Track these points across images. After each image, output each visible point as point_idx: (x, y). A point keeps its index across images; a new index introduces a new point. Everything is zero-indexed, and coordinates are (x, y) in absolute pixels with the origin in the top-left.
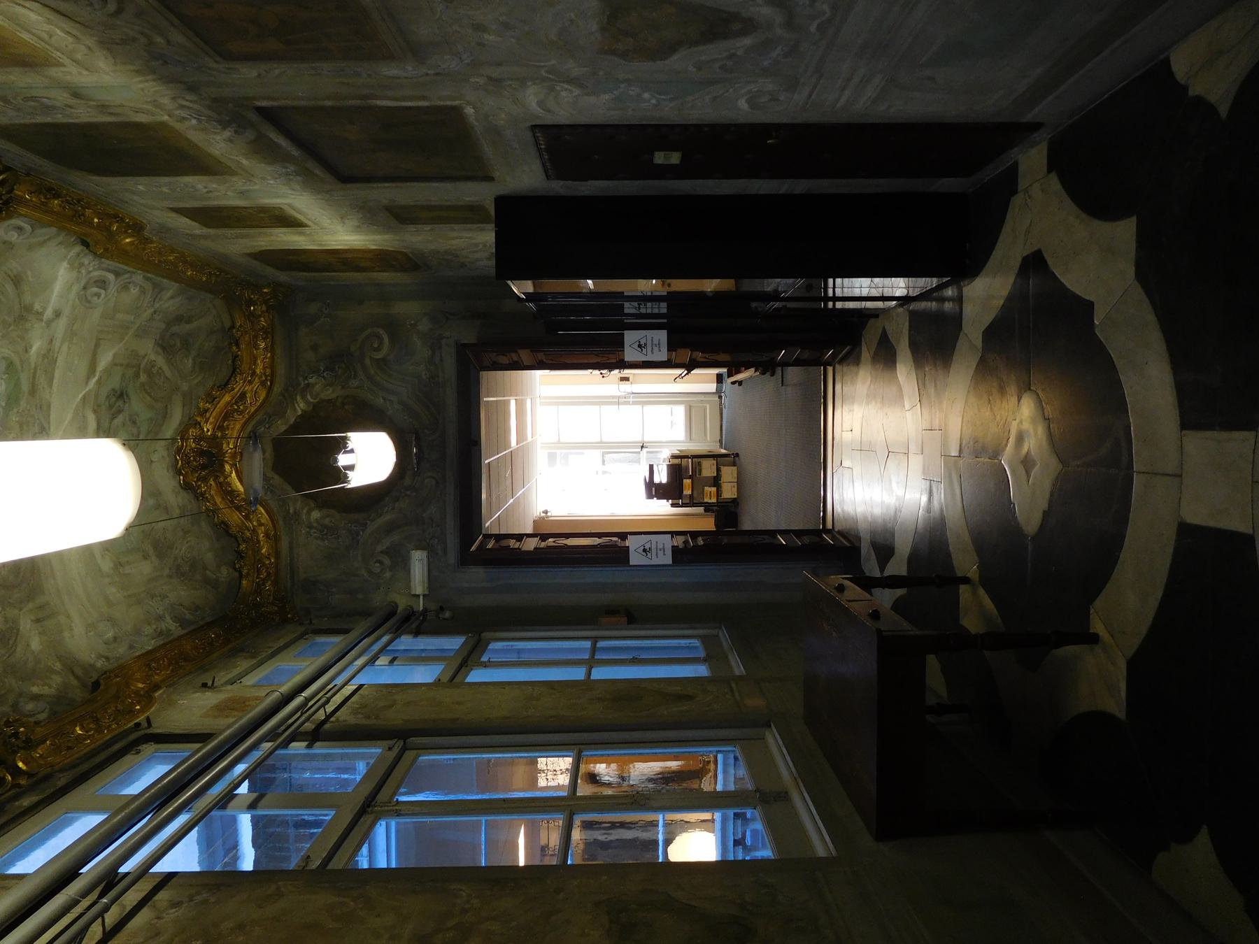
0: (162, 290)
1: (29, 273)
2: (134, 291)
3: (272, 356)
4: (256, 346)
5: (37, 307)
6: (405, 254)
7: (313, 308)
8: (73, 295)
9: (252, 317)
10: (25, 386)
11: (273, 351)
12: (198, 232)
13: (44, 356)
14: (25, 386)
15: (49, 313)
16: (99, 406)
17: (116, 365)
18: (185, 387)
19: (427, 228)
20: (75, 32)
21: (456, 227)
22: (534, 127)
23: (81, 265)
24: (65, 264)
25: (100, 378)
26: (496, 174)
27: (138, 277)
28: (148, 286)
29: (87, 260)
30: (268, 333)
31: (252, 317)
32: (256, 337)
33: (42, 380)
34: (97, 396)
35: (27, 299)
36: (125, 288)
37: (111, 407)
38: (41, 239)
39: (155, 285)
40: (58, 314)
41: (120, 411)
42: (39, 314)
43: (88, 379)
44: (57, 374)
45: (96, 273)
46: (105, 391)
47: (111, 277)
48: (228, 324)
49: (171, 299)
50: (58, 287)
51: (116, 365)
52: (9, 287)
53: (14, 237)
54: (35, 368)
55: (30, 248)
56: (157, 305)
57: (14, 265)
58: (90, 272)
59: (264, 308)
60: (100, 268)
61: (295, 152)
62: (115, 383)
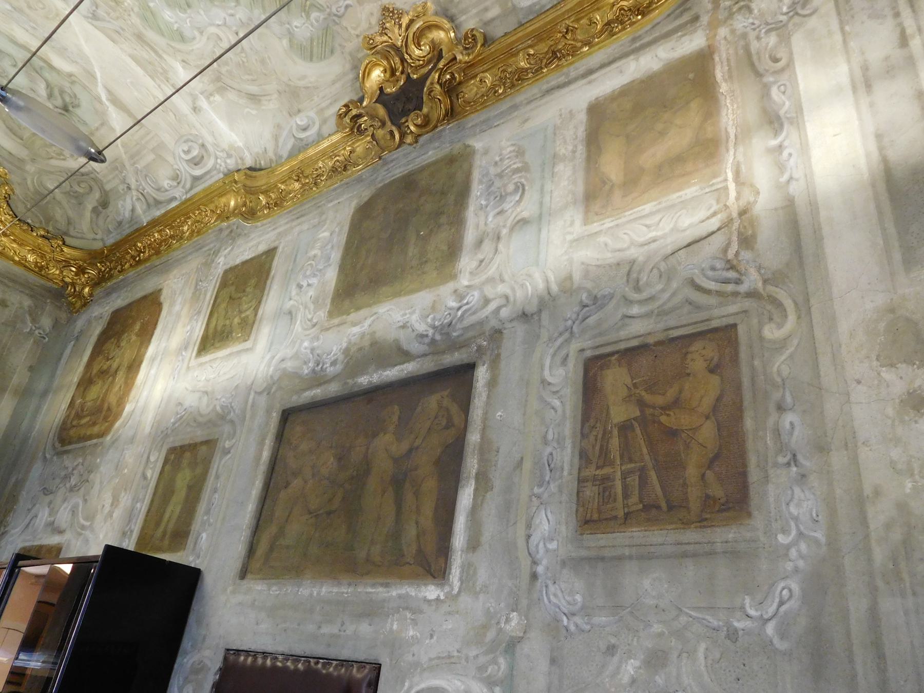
0: (148, 205)
1: (254, 112)
2: (166, 183)
3: (13, 260)
4: (33, 251)
5: (217, 98)
6: (102, 435)
7: (46, 322)
8: (204, 133)
9: (67, 264)
10: (151, 35)
11: (19, 263)
12: (221, 260)
13: (165, 72)
14: (151, 35)
15: (203, 103)
16: (73, 83)
17: (102, 124)
18: (30, 168)
19: (153, 474)
20: (653, 246)
21: (142, 508)
22: (377, 668)
23: (229, 156)
24: (240, 144)
25: (101, 102)
26: (247, 584)
27: (180, 194)
28: (161, 197)
29: (231, 163)
30: (40, 270)
31: (67, 264)
32: (42, 257)
33: (145, 54)
34: (85, 87)
35: (232, 95)
36: (176, 178)
37: (62, 92)
38: (281, 141)
39: (158, 203)
40: (196, 109)
41: (50, 96)
42: (209, 96)
43: (109, 92)
44: (139, 71)
45: (210, 163)
46: (83, 98)
47: (198, 172)
48: (68, 240)
49: (131, 208)
50: (222, 126)
51: (102, 124)
52: (253, 89)
53: (301, 120)
54: (160, 57)
55: (279, 126)
56: (134, 193)
57: (272, 105)
58: (217, 158)
59: (67, 280)
60: (214, 168)
61: (364, 380)
62: (84, 112)
